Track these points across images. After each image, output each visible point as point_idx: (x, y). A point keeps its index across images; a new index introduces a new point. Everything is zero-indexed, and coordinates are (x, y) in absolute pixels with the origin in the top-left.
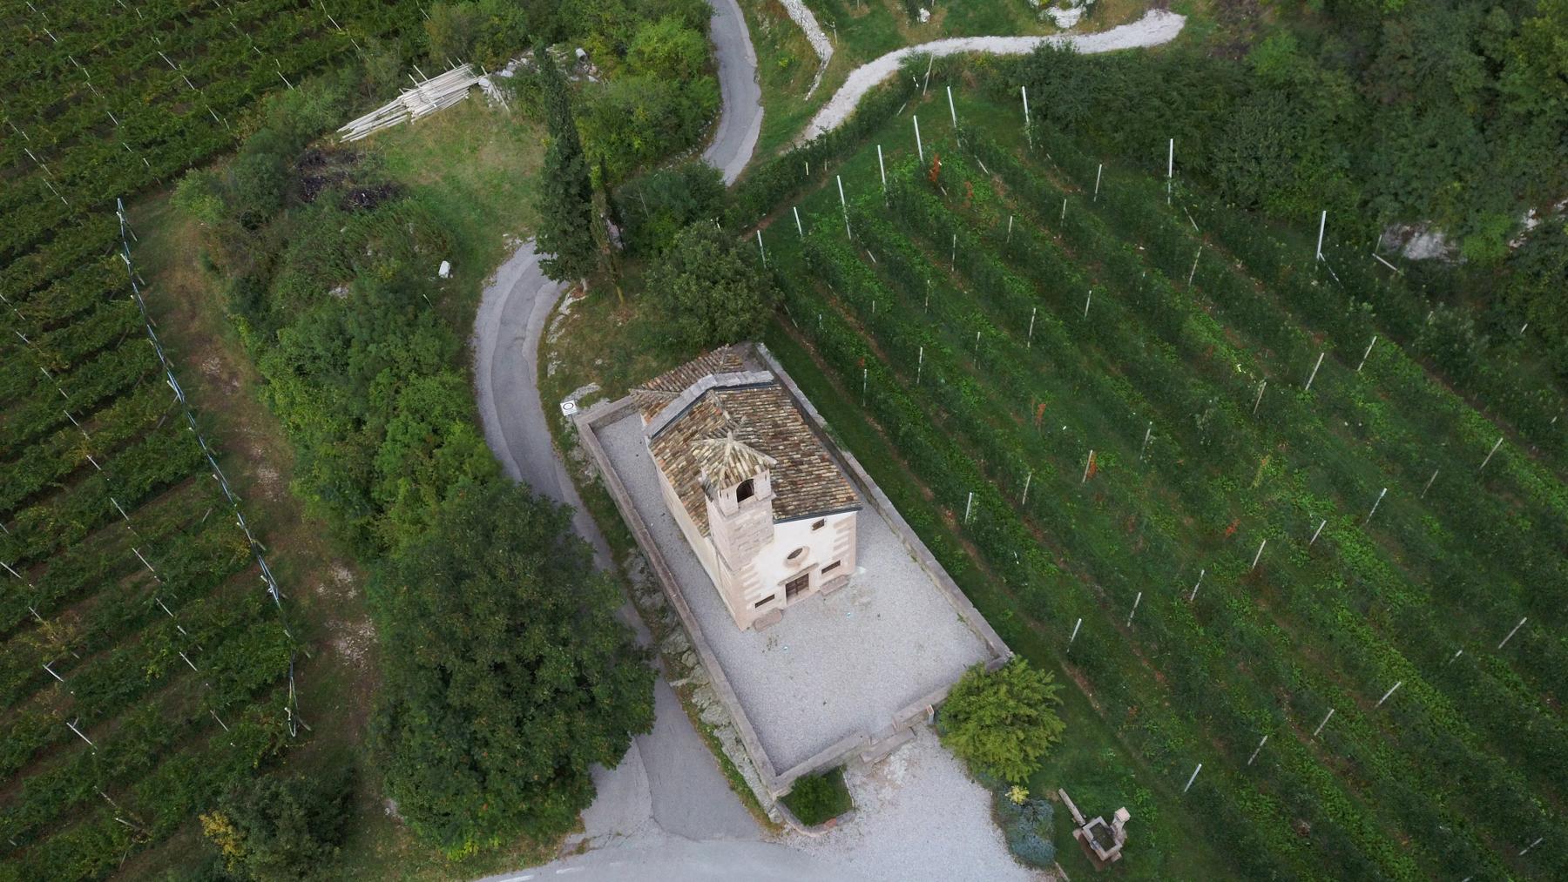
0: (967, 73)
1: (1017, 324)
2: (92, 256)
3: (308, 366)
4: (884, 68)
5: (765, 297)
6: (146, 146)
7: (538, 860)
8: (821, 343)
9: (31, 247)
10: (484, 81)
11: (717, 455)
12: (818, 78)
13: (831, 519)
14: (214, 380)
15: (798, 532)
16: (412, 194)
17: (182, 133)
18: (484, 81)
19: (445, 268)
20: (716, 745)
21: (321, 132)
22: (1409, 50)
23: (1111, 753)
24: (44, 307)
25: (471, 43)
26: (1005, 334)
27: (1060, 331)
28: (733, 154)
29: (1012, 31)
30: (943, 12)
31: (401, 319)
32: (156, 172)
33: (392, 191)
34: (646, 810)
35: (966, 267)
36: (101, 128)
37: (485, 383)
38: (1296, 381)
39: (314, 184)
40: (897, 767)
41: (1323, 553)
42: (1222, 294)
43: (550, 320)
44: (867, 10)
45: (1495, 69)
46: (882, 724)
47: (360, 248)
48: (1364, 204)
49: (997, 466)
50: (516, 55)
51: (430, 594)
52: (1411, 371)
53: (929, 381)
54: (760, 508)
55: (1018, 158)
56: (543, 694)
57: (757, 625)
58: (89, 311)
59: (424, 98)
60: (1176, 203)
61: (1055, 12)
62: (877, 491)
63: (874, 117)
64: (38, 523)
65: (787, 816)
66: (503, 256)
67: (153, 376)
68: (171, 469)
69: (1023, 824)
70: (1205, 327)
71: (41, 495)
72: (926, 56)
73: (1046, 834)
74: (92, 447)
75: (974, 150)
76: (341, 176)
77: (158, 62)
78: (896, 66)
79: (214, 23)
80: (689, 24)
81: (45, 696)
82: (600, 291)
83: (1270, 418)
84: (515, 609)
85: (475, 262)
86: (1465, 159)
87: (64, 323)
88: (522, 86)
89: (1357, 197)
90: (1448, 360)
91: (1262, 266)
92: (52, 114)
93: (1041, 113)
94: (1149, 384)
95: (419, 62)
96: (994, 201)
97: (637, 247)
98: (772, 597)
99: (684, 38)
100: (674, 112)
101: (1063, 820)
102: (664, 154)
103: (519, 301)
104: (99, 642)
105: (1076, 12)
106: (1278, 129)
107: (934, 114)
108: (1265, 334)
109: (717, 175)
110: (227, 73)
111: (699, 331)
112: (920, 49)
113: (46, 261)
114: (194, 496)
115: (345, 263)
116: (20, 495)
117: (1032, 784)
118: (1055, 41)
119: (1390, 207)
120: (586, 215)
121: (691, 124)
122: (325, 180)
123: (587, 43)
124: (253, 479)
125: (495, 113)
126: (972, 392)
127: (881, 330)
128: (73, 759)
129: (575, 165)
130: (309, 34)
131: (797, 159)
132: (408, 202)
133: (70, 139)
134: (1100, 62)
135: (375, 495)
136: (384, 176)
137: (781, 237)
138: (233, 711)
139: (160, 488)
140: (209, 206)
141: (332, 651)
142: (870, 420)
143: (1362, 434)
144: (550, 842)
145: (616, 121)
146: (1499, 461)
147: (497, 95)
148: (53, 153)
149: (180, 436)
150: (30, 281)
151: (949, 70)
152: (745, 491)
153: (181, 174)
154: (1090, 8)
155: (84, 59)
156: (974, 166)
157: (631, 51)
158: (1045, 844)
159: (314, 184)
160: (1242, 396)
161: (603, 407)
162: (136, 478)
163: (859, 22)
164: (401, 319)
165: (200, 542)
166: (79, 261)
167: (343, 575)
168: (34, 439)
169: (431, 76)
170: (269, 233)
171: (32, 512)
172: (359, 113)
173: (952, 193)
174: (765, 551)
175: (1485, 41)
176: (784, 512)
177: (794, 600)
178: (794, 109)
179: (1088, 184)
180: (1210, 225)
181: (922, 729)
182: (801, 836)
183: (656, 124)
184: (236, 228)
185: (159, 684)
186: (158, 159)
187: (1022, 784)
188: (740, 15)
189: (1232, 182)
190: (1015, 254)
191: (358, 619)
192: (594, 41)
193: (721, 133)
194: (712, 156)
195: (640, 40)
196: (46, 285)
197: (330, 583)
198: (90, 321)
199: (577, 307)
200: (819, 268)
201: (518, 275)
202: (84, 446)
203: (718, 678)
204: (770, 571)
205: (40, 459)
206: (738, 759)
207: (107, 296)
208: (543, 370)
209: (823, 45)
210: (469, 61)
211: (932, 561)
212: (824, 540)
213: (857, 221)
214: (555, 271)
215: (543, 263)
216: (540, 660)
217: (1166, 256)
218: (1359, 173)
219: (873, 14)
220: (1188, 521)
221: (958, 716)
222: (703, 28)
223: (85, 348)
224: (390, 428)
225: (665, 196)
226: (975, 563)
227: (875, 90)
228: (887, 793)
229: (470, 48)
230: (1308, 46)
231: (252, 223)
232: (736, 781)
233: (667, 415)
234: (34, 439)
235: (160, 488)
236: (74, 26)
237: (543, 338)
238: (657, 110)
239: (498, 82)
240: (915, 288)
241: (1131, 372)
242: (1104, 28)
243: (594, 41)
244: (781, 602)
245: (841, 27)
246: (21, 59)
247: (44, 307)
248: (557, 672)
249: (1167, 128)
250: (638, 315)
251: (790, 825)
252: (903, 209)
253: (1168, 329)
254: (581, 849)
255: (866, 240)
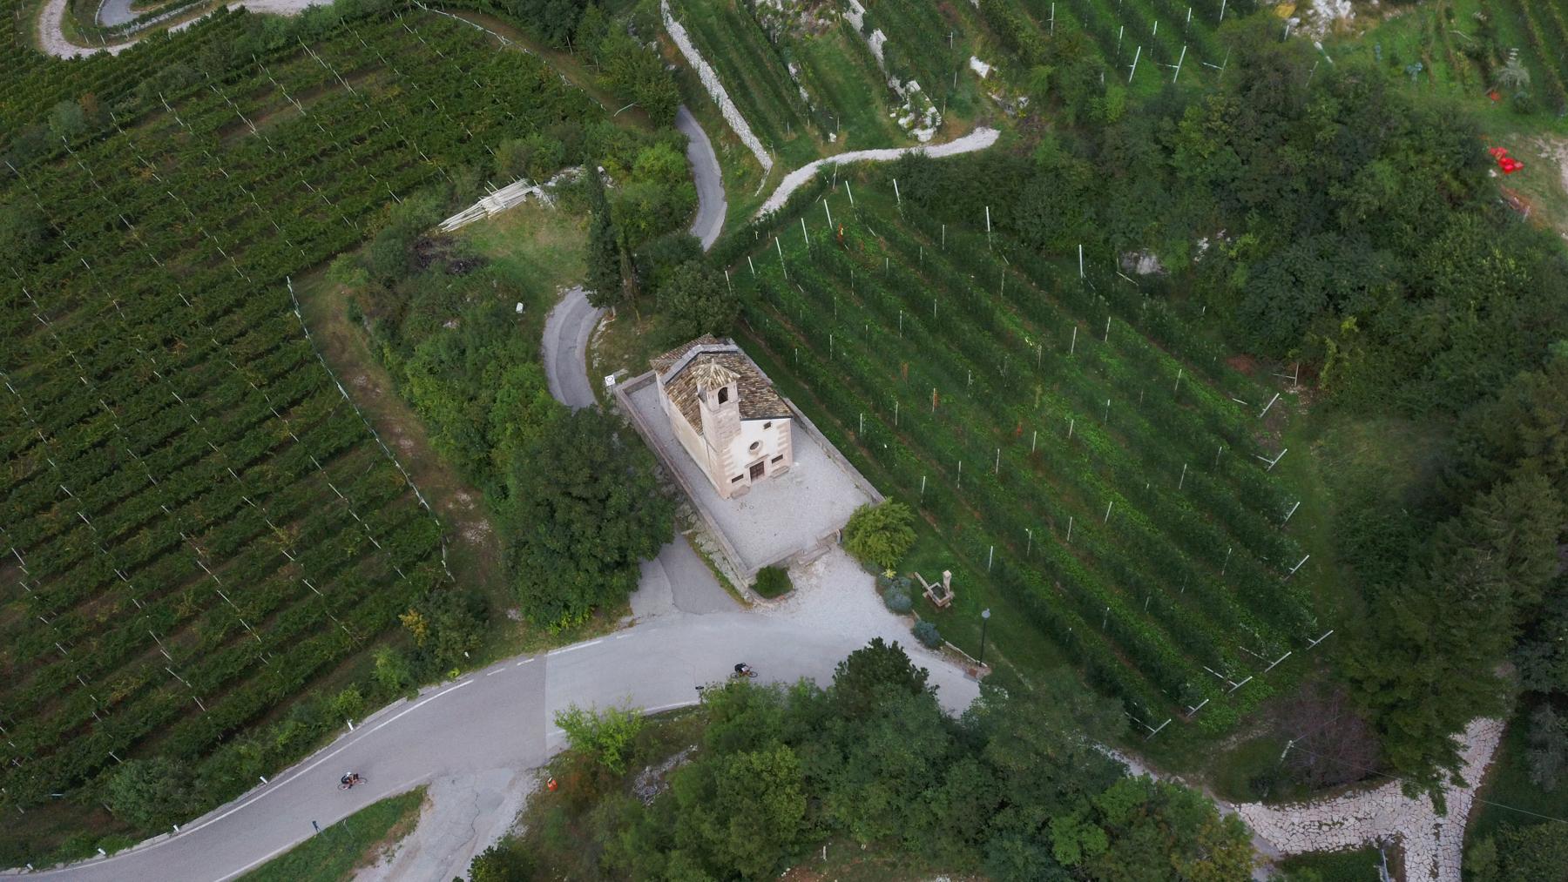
0: (861, 174)
1: (892, 322)
2: (272, 314)
3: (437, 368)
4: (807, 172)
5: (732, 308)
6: (301, 243)
7: (605, 632)
8: (768, 340)
9: (227, 311)
10: (536, 190)
11: (707, 373)
12: (763, 181)
13: (775, 422)
14: (363, 389)
15: (753, 429)
16: (493, 262)
17: (325, 233)
18: (536, 190)
19: (520, 307)
20: (710, 563)
21: (427, 227)
22: (1120, 143)
23: (946, 553)
24: (243, 347)
25: (527, 166)
26: (886, 330)
27: (922, 331)
28: (709, 229)
29: (890, 145)
30: (845, 135)
31: (500, 332)
32: (313, 258)
33: (481, 262)
34: (669, 600)
35: (859, 291)
36: (268, 231)
37: (553, 374)
38: (1064, 350)
39: (426, 259)
40: (819, 567)
41: (1076, 442)
42: (1017, 297)
43: (592, 336)
44: (795, 135)
45: (1168, 151)
46: (811, 543)
47: (462, 296)
48: (1106, 241)
49: (881, 406)
50: (557, 173)
51: (543, 461)
52: (1131, 335)
53: (836, 356)
54: (731, 410)
55: (895, 225)
56: (611, 513)
57: (734, 496)
58: (278, 347)
59: (495, 202)
60: (995, 249)
61: (917, 131)
62: (806, 419)
63: (800, 203)
64: (262, 474)
65: (754, 594)
66: (558, 299)
67: (328, 383)
68: (347, 438)
69: (892, 590)
70: (1008, 319)
71: (263, 459)
72: (833, 163)
73: (906, 593)
74: (292, 428)
75: (866, 221)
76: (444, 253)
77: (303, 188)
78: (815, 170)
79: (339, 160)
80: (674, 148)
81: (283, 571)
82: (624, 316)
83: (1046, 369)
84: (592, 464)
85: (540, 304)
86: (1158, 208)
87: (261, 355)
88: (565, 192)
89: (1102, 236)
90: (1159, 333)
91: (1046, 283)
92: (231, 224)
93: (908, 195)
94: (974, 354)
95: (491, 179)
96: (879, 253)
97: (647, 287)
98: (741, 477)
99: (671, 157)
100: (667, 204)
101: (917, 588)
102: (660, 232)
103: (572, 322)
104: (316, 538)
105: (930, 131)
106: (1050, 196)
107: (838, 201)
108: (1043, 320)
109: (698, 241)
110: (352, 193)
111: (691, 327)
112: (830, 159)
113: (239, 318)
114: (364, 454)
115: (452, 306)
116: (247, 459)
117: (899, 569)
118: (914, 151)
119: (1120, 241)
120: (617, 263)
121: (678, 211)
122: (435, 256)
123: (605, 163)
124: (397, 446)
125: (545, 210)
126: (866, 363)
127: (806, 329)
128: (309, 600)
129: (610, 231)
130: (407, 164)
131: (749, 231)
132: (491, 268)
133: (248, 240)
134: (943, 162)
135: (489, 437)
136: (473, 252)
137: (741, 277)
138: (407, 568)
139: (340, 452)
140: (359, 274)
141: (463, 539)
142: (801, 384)
143: (1104, 376)
144: (611, 622)
145: (630, 210)
146: (1183, 384)
147: (546, 198)
148: (235, 250)
149: (350, 418)
150: (234, 331)
151: (849, 172)
152: (723, 397)
153: (334, 257)
154: (939, 128)
155: (250, 187)
156: (866, 231)
157: (635, 166)
158: (906, 599)
159: (426, 259)
160: (1030, 357)
161: (631, 381)
162: (323, 446)
163: (790, 143)
164: (500, 332)
165: (370, 480)
166: (264, 318)
167: (464, 497)
168: (251, 426)
169: (500, 188)
170: (401, 289)
171: (257, 468)
172: (452, 214)
173: (852, 248)
174: (736, 440)
175: (1161, 136)
176: (746, 415)
177: (756, 481)
178: (747, 202)
179: (938, 239)
180: (1014, 260)
181: (834, 546)
182: (765, 607)
183: (655, 213)
184: (379, 287)
185: (354, 560)
186: (311, 250)
187: (892, 567)
188: (708, 143)
189: (1027, 231)
190: (893, 284)
191: (477, 519)
192: (611, 162)
193: (699, 219)
194: (694, 231)
195: (641, 159)
196: (242, 334)
197: (456, 502)
198: (278, 354)
199: (609, 326)
200: (766, 296)
201: (568, 311)
202: (286, 429)
203: (712, 523)
204: (741, 460)
205: (256, 438)
206: (724, 568)
207: (286, 339)
208: (589, 365)
209: (766, 159)
210: (525, 176)
211: (839, 455)
212: (773, 436)
213: (789, 264)
214: (597, 302)
215: (588, 296)
216: (609, 496)
217: (987, 281)
218: (1102, 222)
219: (799, 138)
220: (996, 431)
221: (856, 538)
222: (683, 151)
223: (277, 370)
224: (499, 396)
225: (665, 251)
226: (865, 454)
227: (801, 187)
228: (814, 581)
229: (521, 170)
230: (1065, 144)
231: (390, 284)
232: (724, 581)
233: (674, 370)
234: (251, 426)
235: (340, 452)
236: (237, 167)
237: (588, 347)
238: (656, 202)
239: (547, 190)
240: (828, 305)
241: (964, 349)
242: (948, 140)
243: (611, 162)
244: (746, 481)
245: (777, 148)
246: (205, 190)
247: (243, 347)
248: (620, 498)
249: (984, 200)
250: (649, 327)
251: (758, 601)
252: (820, 258)
253: (986, 321)
254: (631, 625)
255: (796, 277)
